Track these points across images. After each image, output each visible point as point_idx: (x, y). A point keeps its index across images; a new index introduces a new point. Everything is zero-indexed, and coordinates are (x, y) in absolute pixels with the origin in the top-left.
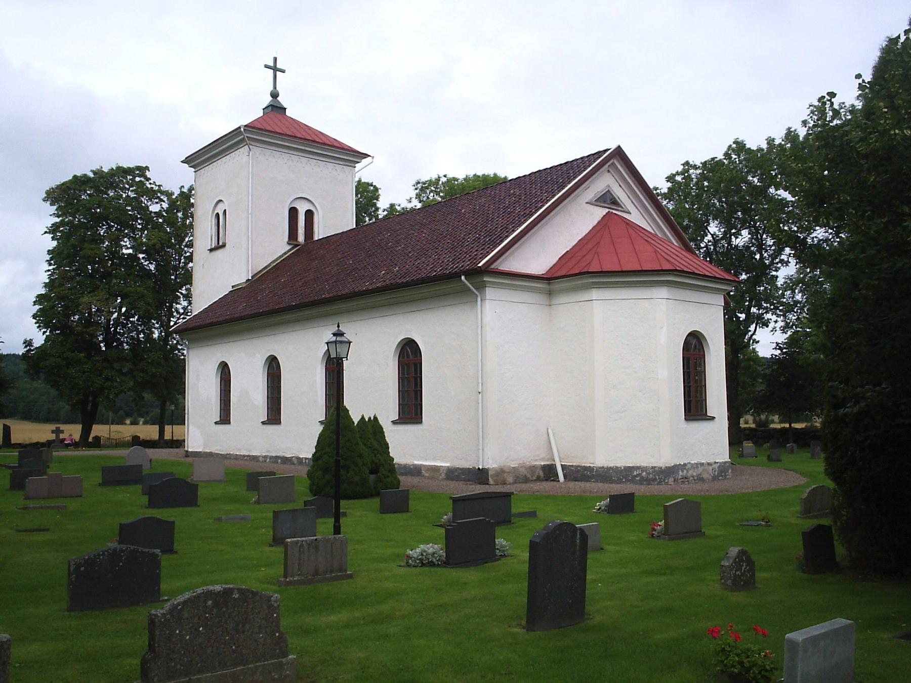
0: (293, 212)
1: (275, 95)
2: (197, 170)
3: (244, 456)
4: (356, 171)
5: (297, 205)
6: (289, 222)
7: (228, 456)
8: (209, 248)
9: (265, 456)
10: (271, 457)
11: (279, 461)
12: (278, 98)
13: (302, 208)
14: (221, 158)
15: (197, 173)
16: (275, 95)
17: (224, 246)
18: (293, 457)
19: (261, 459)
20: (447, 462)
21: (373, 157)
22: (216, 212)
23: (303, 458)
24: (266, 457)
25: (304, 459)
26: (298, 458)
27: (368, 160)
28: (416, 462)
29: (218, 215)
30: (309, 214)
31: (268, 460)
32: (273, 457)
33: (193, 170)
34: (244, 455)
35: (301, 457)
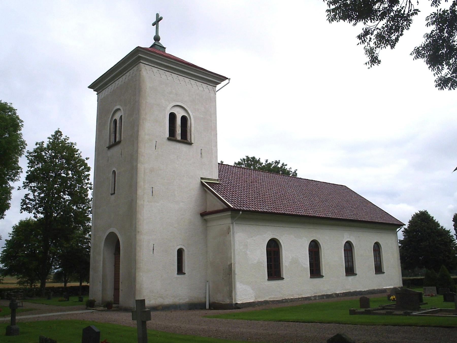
0: (172, 117)
1: (157, 39)
2: (99, 92)
3: (299, 298)
4: (217, 90)
5: (175, 111)
6: (94, 178)
7: (284, 301)
8: (108, 146)
9: (314, 296)
10: (319, 296)
11: (325, 297)
12: (159, 42)
13: (179, 114)
14: (121, 76)
15: (99, 95)
16: (157, 39)
17: (120, 142)
18: (333, 294)
19: (312, 298)
20: (392, 286)
21: (229, 79)
22: (114, 119)
23: (339, 293)
24: (315, 296)
25: (340, 294)
26: (336, 294)
27: (227, 80)
28: (384, 288)
29: (115, 121)
30: (184, 119)
31: (317, 298)
32: (320, 296)
33: (96, 93)
34: (298, 298)
35: (338, 293)
